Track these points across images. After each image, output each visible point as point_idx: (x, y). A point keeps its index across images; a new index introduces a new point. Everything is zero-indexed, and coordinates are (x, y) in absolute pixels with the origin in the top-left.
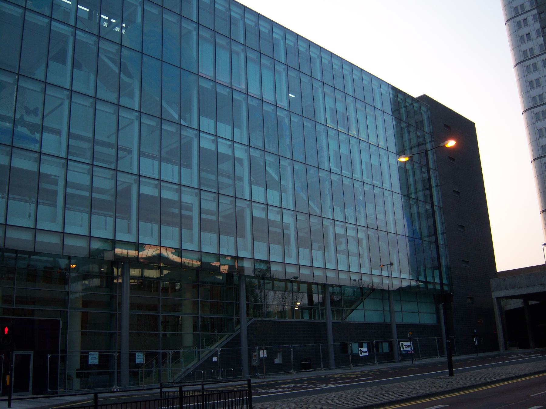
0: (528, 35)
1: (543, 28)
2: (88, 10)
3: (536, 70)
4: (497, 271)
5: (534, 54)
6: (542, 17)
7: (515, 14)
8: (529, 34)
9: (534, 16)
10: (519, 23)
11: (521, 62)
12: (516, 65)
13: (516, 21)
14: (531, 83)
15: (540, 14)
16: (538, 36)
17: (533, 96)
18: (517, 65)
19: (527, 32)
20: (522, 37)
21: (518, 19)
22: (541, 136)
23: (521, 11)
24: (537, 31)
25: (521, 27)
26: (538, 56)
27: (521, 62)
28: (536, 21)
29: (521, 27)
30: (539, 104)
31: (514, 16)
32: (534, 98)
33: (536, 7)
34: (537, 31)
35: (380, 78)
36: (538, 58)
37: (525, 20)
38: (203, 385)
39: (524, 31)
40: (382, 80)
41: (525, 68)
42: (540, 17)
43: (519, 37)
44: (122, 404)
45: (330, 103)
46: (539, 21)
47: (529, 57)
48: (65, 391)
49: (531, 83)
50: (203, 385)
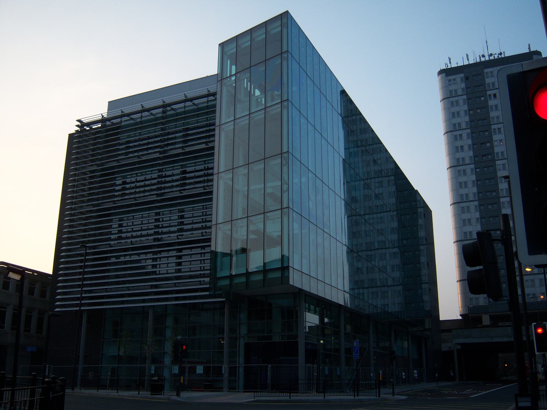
0: (462, 147)
1: (468, 99)
2: (32, 273)
3: (462, 151)
4: (441, 319)
6: (481, 208)
9: (464, 100)
10: (456, 136)
11: (448, 98)
12: (450, 167)
13: (454, 134)
14: (460, 183)
15: (468, 99)
16: (477, 222)
18: (454, 204)
21: (455, 133)
22: (464, 225)
24: (469, 145)
26: (464, 129)
27: (448, 98)
28: (470, 150)
30: (465, 200)
31: (449, 97)
34: (469, 145)
37: (461, 135)
39: (459, 143)
40: (321, 57)
42: (473, 148)
43: (453, 135)
44: (192, 216)
48: (120, 221)
49: (460, 183)
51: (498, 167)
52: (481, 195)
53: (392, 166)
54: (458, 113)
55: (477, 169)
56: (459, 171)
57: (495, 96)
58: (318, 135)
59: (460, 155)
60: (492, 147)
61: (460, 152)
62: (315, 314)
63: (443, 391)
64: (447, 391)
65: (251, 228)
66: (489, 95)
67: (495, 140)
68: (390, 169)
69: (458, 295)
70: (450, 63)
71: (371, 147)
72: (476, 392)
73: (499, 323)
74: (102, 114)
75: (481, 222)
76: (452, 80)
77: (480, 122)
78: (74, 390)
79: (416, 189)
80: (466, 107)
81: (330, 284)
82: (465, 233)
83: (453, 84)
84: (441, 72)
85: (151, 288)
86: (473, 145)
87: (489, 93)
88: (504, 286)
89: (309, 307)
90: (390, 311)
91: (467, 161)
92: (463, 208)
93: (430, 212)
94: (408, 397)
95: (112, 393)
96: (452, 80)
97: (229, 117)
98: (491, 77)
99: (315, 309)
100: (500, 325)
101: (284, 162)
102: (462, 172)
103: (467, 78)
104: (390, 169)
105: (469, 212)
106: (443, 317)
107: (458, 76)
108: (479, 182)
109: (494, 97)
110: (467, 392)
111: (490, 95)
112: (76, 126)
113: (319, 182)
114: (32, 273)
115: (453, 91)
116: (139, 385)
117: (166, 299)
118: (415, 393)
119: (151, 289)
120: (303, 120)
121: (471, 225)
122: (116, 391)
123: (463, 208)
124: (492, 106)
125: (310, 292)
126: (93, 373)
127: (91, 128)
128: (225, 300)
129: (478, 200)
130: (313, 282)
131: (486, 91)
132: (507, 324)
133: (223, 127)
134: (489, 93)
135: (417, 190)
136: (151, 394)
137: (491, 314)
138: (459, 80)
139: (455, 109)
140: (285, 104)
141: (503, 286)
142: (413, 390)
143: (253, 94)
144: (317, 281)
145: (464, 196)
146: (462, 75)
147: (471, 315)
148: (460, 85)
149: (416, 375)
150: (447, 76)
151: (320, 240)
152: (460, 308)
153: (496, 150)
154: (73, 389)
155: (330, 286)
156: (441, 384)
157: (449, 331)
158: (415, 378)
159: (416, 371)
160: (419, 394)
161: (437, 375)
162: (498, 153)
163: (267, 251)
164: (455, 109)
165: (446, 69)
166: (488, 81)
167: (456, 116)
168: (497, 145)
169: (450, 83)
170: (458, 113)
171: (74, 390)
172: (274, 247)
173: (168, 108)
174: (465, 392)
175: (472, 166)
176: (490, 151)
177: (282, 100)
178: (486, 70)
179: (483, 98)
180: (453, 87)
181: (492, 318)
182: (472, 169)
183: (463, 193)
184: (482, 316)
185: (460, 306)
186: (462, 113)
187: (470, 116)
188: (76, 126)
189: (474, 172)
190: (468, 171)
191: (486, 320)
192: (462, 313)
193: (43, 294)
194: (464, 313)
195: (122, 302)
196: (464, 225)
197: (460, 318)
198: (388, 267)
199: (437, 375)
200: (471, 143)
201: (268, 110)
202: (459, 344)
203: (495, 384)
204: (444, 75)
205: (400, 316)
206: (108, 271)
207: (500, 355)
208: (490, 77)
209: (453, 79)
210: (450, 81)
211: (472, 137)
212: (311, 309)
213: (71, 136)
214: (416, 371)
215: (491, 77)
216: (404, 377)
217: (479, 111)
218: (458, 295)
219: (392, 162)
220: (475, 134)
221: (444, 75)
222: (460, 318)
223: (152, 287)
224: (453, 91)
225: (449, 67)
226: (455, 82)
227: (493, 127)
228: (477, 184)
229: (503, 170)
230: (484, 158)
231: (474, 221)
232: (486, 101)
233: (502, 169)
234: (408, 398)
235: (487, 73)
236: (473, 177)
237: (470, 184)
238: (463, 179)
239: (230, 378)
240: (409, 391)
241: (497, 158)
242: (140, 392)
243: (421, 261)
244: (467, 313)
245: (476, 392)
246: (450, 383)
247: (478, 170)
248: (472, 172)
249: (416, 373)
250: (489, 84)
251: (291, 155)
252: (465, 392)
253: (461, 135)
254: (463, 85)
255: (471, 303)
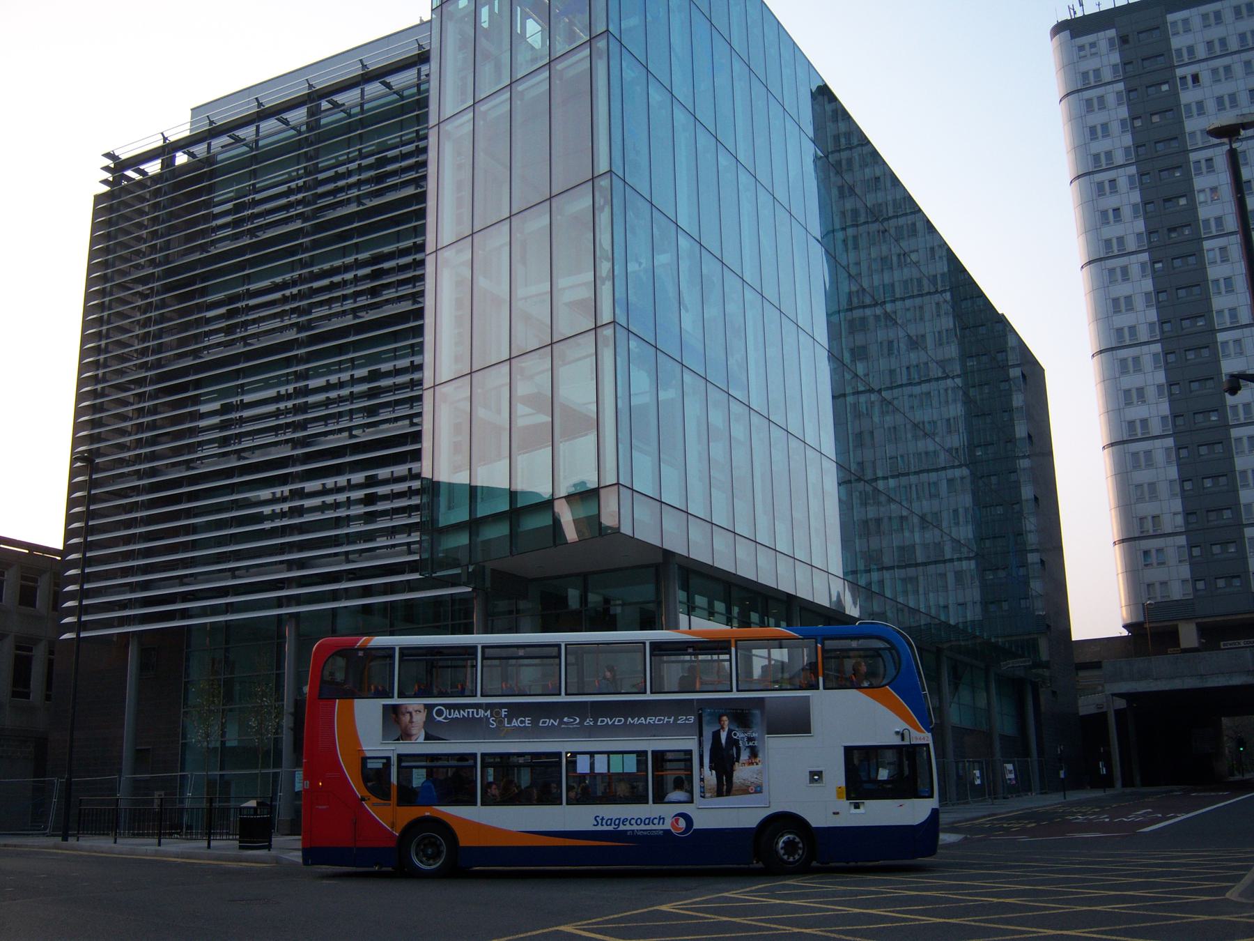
0: (1116, 210)
2: (27, 551)
5: (1113, 163)
7: (1095, 167)
8: (1119, 209)
10: (1100, 186)
11: (1078, 91)
15: (1129, 91)
16: (1160, 394)
17: (1127, 387)
19: (1115, 206)
20: (1104, 213)
21: (1099, 177)
22: (1128, 403)
23: (1095, 82)
24: (1135, 206)
25: (1093, 111)
26: (1109, 83)
27: (1078, 91)
28: (1138, 217)
29: (1105, 194)
30: (1128, 342)
32: (1119, 331)
33: (1149, 248)
34: (1135, 206)
35: (796, 41)
36: (1133, 258)
37: (1113, 182)
38: (395, 355)
39: (1110, 202)
41: (1106, 273)
45: (693, 408)
46: (1140, 190)
47: (1104, 167)
49: (1116, 301)
50: (395, 355)
51: (1208, 256)
52: (1167, 327)
53: (942, 267)
54: (1105, 126)
55: (1158, 262)
56: (1112, 271)
57: (1196, 78)
58: (704, 140)
59: (1113, 231)
60: (1192, 207)
61: (1112, 222)
62: (709, 620)
63: (1073, 814)
64: (1084, 814)
65: (522, 389)
66: (1180, 78)
67: (1199, 188)
68: (905, 227)
69: (1118, 578)
70: (1081, 5)
71: (893, 223)
72: (1160, 815)
73: (1222, 643)
74: (162, 134)
75: (1171, 394)
76: (1087, 47)
77: (1160, 146)
78: (67, 840)
79: (1000, 312)
80: (1123, 112)
81: (684, 509)
82: (1131, 424)
83: (1091, 55)
84: (1060, 28)
85: (290, 570)
86: (1145, 203)
87: (1179, 72)
88: (1233, 550)
89: (711, 605)
90: (952, 622)
91: (1131, 245)
92: (1123, 361)
93: (1041, 371)
94: (963, 836)
95: (145, 846)
96: (1087, 47)
97: (463, 101)
98: (1184, 32)
99: (711, 605)
100: (1222, 647)
101: (600, 201)
102: (1118, 271)
103: (1124, 40)
104: (905, 227)
105: (1140, 370)
106: (1079, 632)
107: (1101, 34)
108: (1162, 297)
109: (1194, 82)
110: (1137, 816)
111: (1183, 78)
112: (103, 168)
113: (710, 267)
114: (27, 551)
115: (1091, 73)
116: (211, 826)
117: (335, 596)
118: (995, 822)
119: (288, 571)
120: (656, 96)
121: (1144, 402)
122: (156, 841)
123: (1123, 361)
124: (1188, 106)
125: (688, 558)
126: (163, 793)
127: (143, 173)
128: (470, 589)
129: (1150, 250)
130: (784, 565)
131: (1173, 67)
132: (1243, 645)
133: (447, 127)
134: (1179, 72)
135: (1003, 315)
136: (241, 848)
137: (1200, 620)
138: (1103, 45)
139: (1097, 118)
140: (601, 44)
141: (1230, 551)
142: (994, 815)
143: (519, 32)
144: (659, 507)
145: (1126, 332)
146: (1112, 33)
147: (1151, 625)
148: (1107, 58)
149: (1012, 776)
150: (1073, 37)
151: (717, 418)
152: (1124, 609)
153: (1204, 213)
154: (65, 839)
155: (792, 560)
156: (1074, 796)
157: (1097, 665)
158: (1008, 782)
159: (1010, 767)
160: (1005, 825)
161: (1062, 775)
162: (1207, 221)
163: (562, 447)
164: (1097, 118)
165: (1072, 19)
166: (1176, 43)
167: (1096, 109)
168: (1205, 202)
169: (1082, 53)
170: (1105, 126)
171: (67, 840)
172: (582, 436)
173: (325, 105)
174: (1131, 818)
175: (1145, 257)
176: (1190, 218)
177: (593, 35)
178: (1171, 18)
179: (1165, 88)
180: (1090, 64)
181: (1203, 630)
182: (1143, 265)
183: (1122, 326)
184: (1177, 626)
185: (1123, 605)
186: (1115, 127)
187: (1134, 132)
188: (103, 168)
189: (1150, 272)
190: (1135, 270)
191: (1189, 635)
192: (1129, 621)
193: (27, 597)
194: (1134, 621)
195: (229, 608)
196: (1128, 403)
197: (1125, 633)
198: (945, 515)
199: (1062, 775)
200: (1138, 200)
201: (559, 66)
202: (1120, 695)
203: (1213, 794)
204: (1067, 33)
205: (978, 634)
206: (193, 529)
207: (1225, 721)
208: (1181, 32)
209: (1090, 44)
210: (1081, 48)
211: (1130, 100)
212: (716, 610)
213: (98, 199)
214: (1010, 767)
215: (1184, 32)
216: (978, 782)
217: (1156, 119)
218: (1118, 578)
219: (940, 246)
220: (1177, 386)
221: (1067, 33)
222: (1125, 633)
223: (291, 565)
224: (1091, 73)
225: (1079, 14)
226: (1094, 50)
227: (1193, 157)
228: (1158, 302)
229: (1222, 261)
230: (1173, 235)
231: (1151, 392)
232: (1175, 94)
233: (1219, 260)
234: (966, 838)
235: (1174, 23)
236: (1148, 285)
237: (1139, 302)
238: (1122, 290)
239: (297, 803)
240: (984, 817)
241: (1205, 233)
242: (213, 843)
243: (1023, 498)
244: (1142, 619)
245: (1160, 815)
246: (1098, 794)
247: (1158, 265)
248: (1168, 456)
249: (1010, 772)
250: (1179, 51)
251: (622, 183)
252: (1131, 818)
253: (1113, 182)
254: (1115, 58)
255: (1149, 594)
